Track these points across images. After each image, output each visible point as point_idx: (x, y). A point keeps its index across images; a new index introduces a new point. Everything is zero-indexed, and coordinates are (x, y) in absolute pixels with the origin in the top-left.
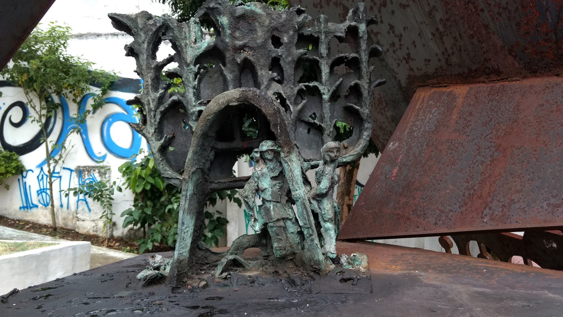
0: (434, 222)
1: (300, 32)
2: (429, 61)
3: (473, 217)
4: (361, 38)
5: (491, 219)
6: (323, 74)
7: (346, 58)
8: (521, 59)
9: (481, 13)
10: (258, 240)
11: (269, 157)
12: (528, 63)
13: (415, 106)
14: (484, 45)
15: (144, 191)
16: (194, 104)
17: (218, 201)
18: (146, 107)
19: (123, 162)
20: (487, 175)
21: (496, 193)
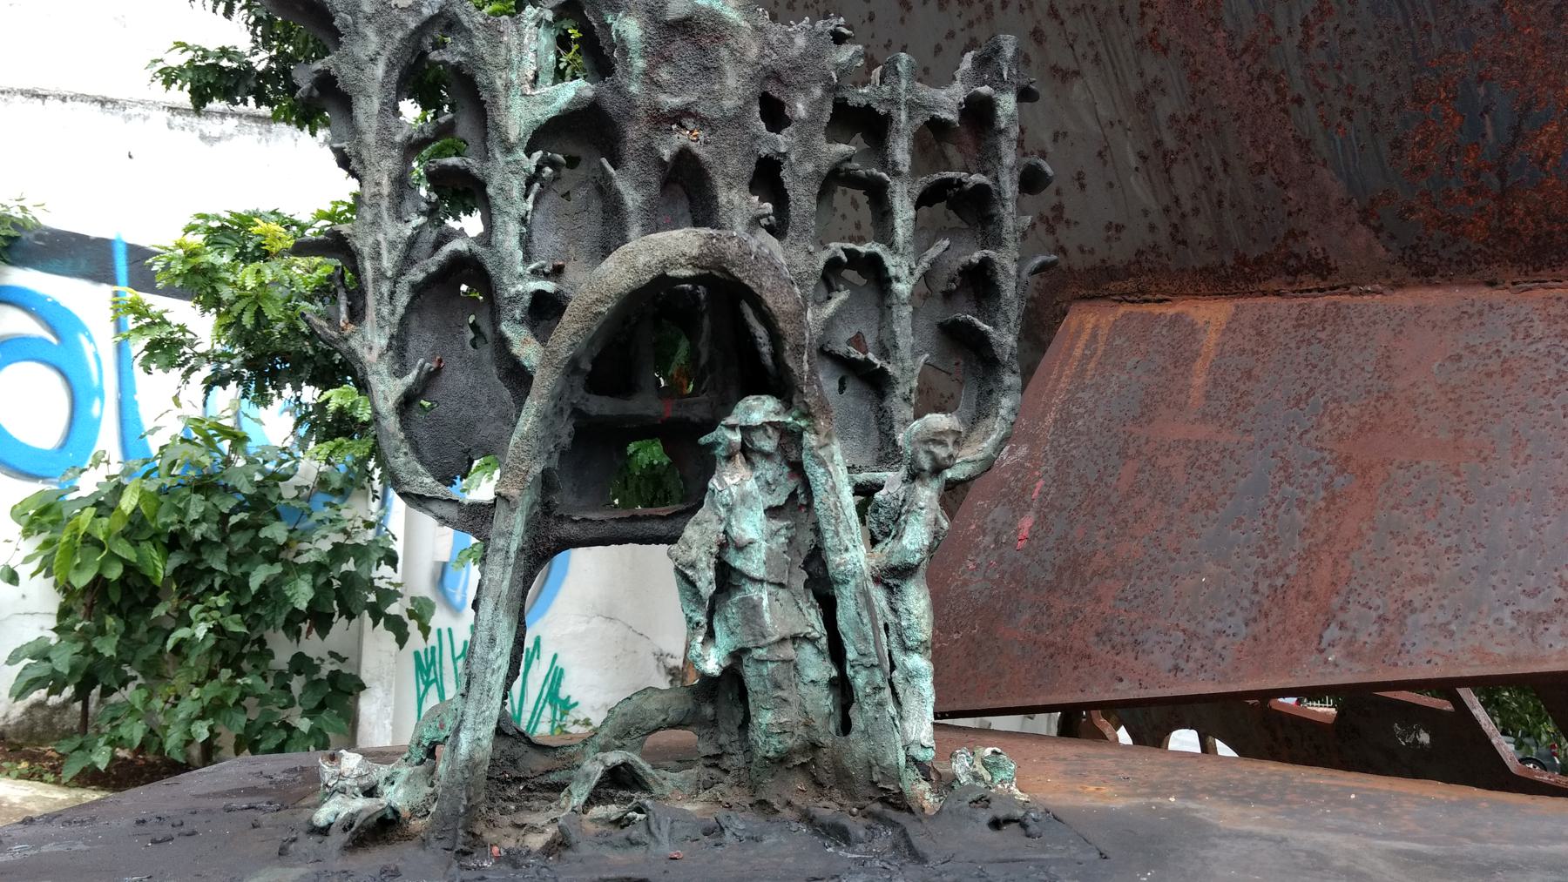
0: (1170, 663)
1: (839, 95)
2: (1119, 228)
3: (1292, 651)
4: (1001, 132)
5: (1350, 655)
6: (898, 222)
7: (960, 183)
8: (1393, 237)
9: (1294, 108)
10: (690, 705)
11: (768, 444)
12: (1414, 248)
13: (1072, 347)
14: (1290, 194)
15: (99, 583)
16: (520, 269)
17: (340, 623)
18: (368, 265)
19: (30, 489)
20: (1321, 536)
21: (1354, 584)
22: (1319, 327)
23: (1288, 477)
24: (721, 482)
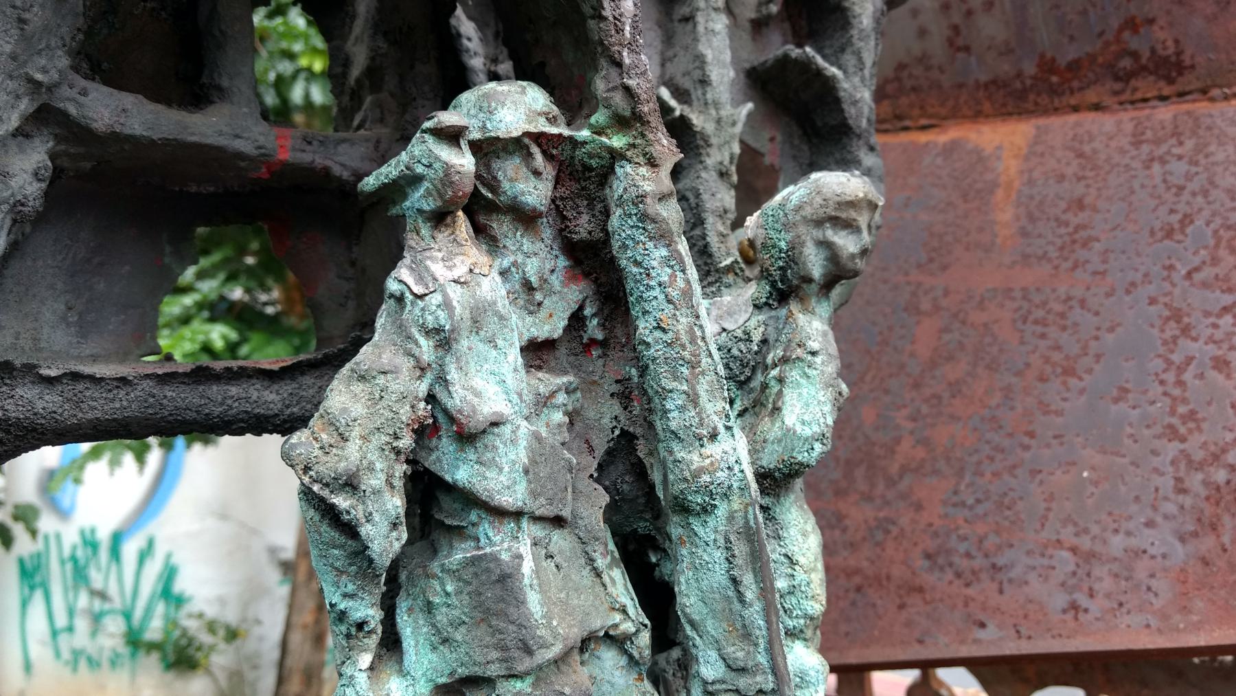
22: (1174, 141)
23: (1186, 331)
24: (421, 273)
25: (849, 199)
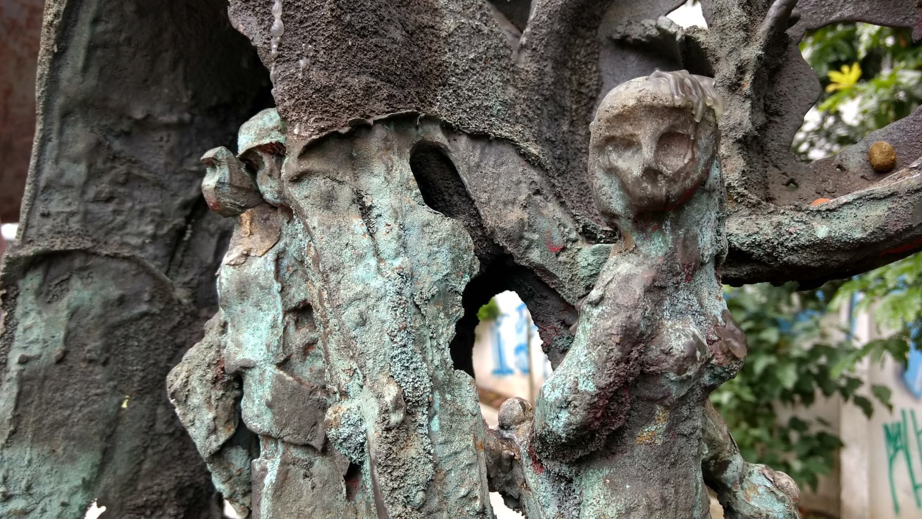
25: (616, 112)
